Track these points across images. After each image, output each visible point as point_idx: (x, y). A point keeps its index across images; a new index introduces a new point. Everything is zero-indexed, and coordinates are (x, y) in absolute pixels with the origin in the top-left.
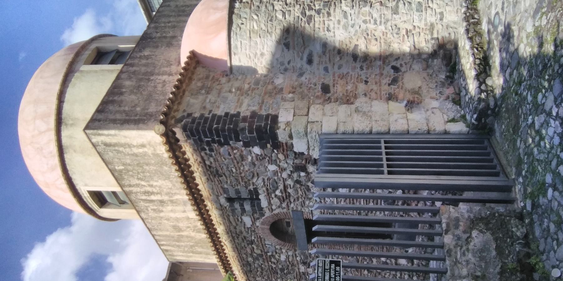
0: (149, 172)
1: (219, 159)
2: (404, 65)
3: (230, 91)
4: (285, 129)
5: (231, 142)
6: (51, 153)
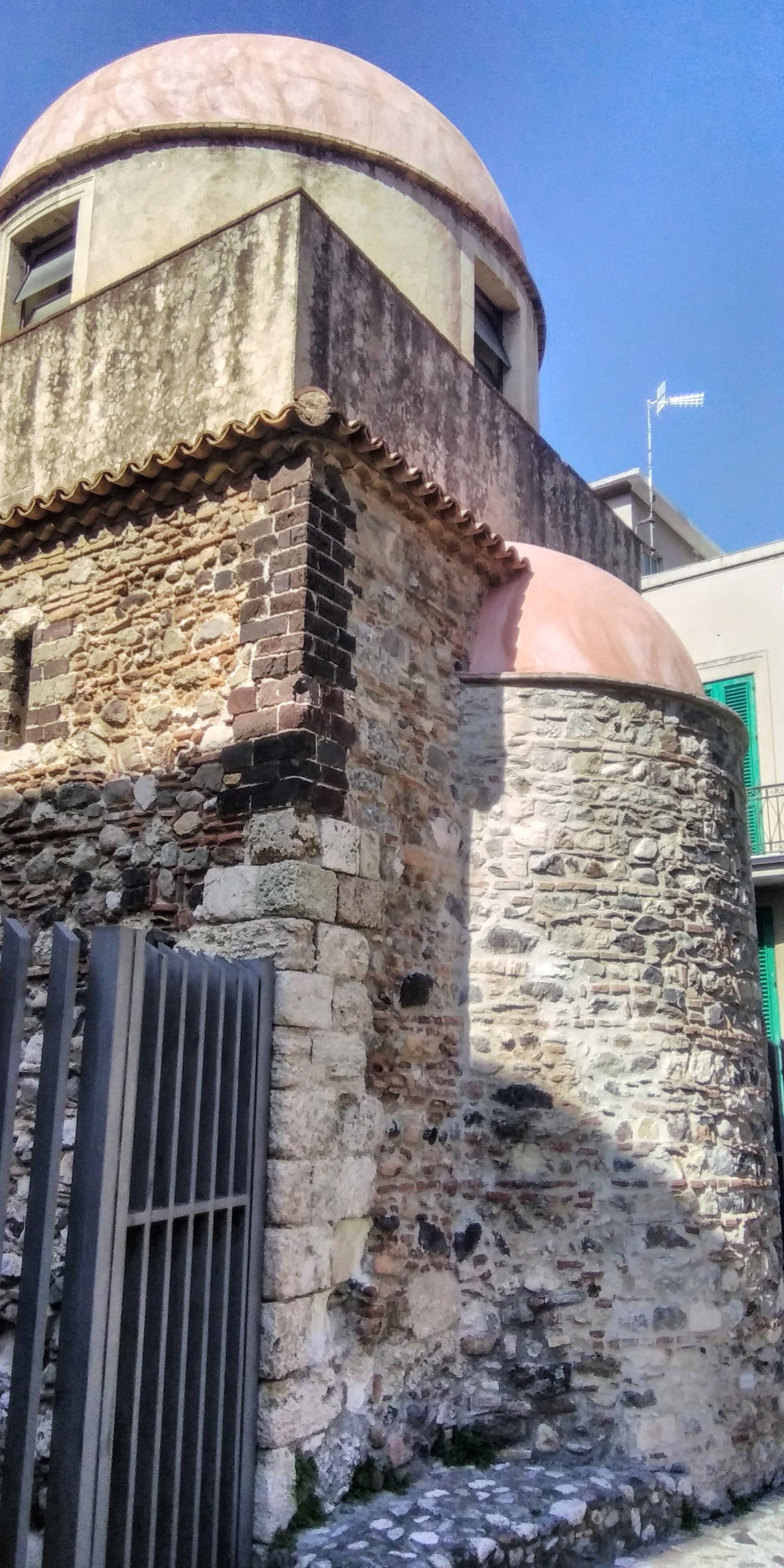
0: (140, 387)
1: (189, 607)
2: (483, 1269)
3: (413, 669)
4: (295, 835)
5: (253, 648)
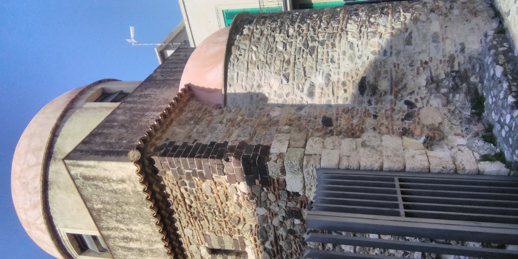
0: (128, 213)
1: (201, 197)
2: (419, 100)
3: (221, 122)
4: (276, 161)
5: (214, 176)
6: (36, 188)
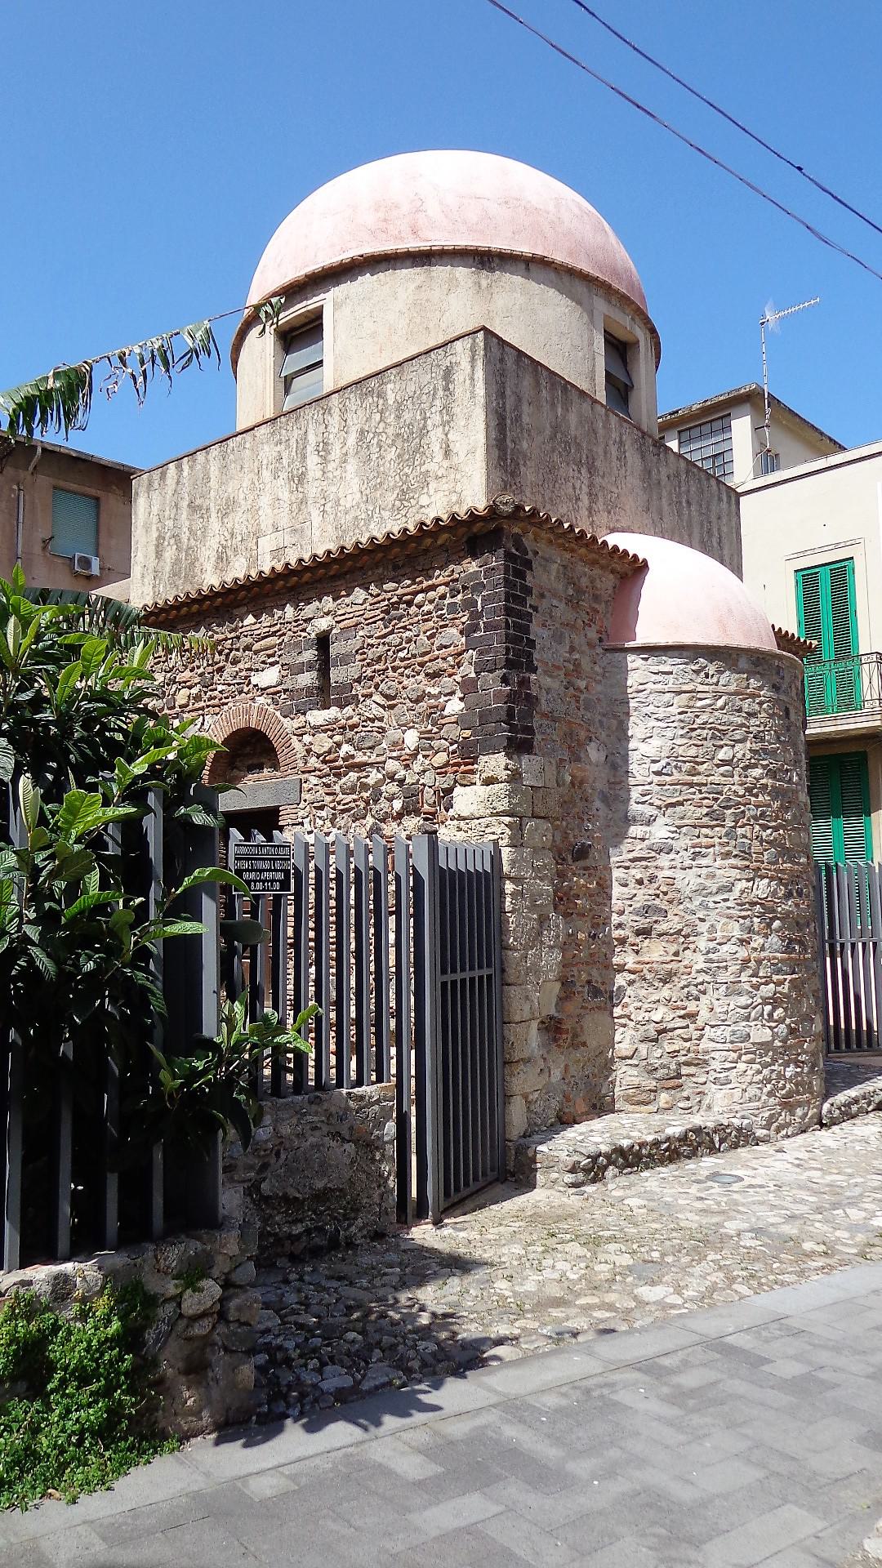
1: (431, 624)
3: (572, 649)
